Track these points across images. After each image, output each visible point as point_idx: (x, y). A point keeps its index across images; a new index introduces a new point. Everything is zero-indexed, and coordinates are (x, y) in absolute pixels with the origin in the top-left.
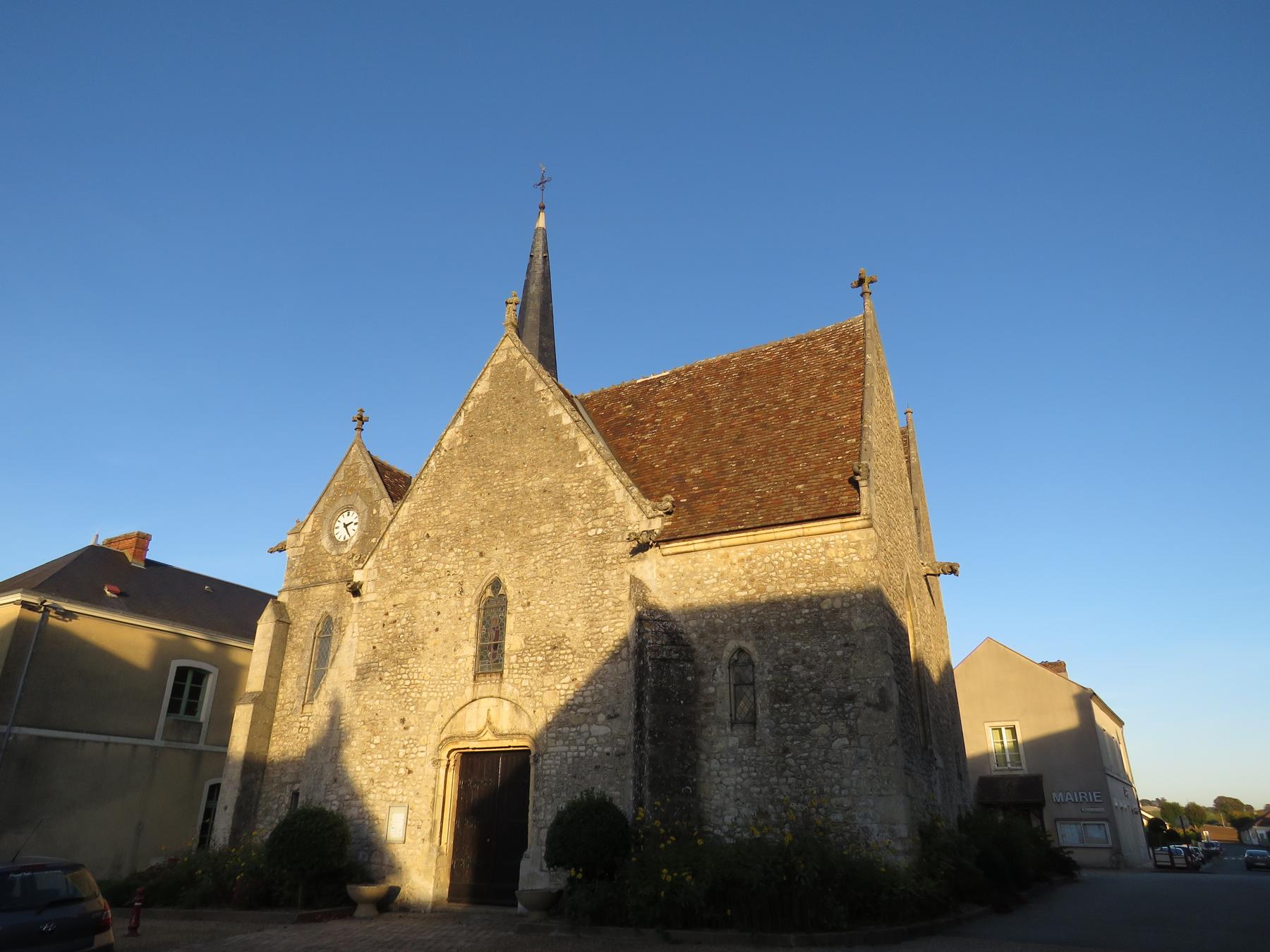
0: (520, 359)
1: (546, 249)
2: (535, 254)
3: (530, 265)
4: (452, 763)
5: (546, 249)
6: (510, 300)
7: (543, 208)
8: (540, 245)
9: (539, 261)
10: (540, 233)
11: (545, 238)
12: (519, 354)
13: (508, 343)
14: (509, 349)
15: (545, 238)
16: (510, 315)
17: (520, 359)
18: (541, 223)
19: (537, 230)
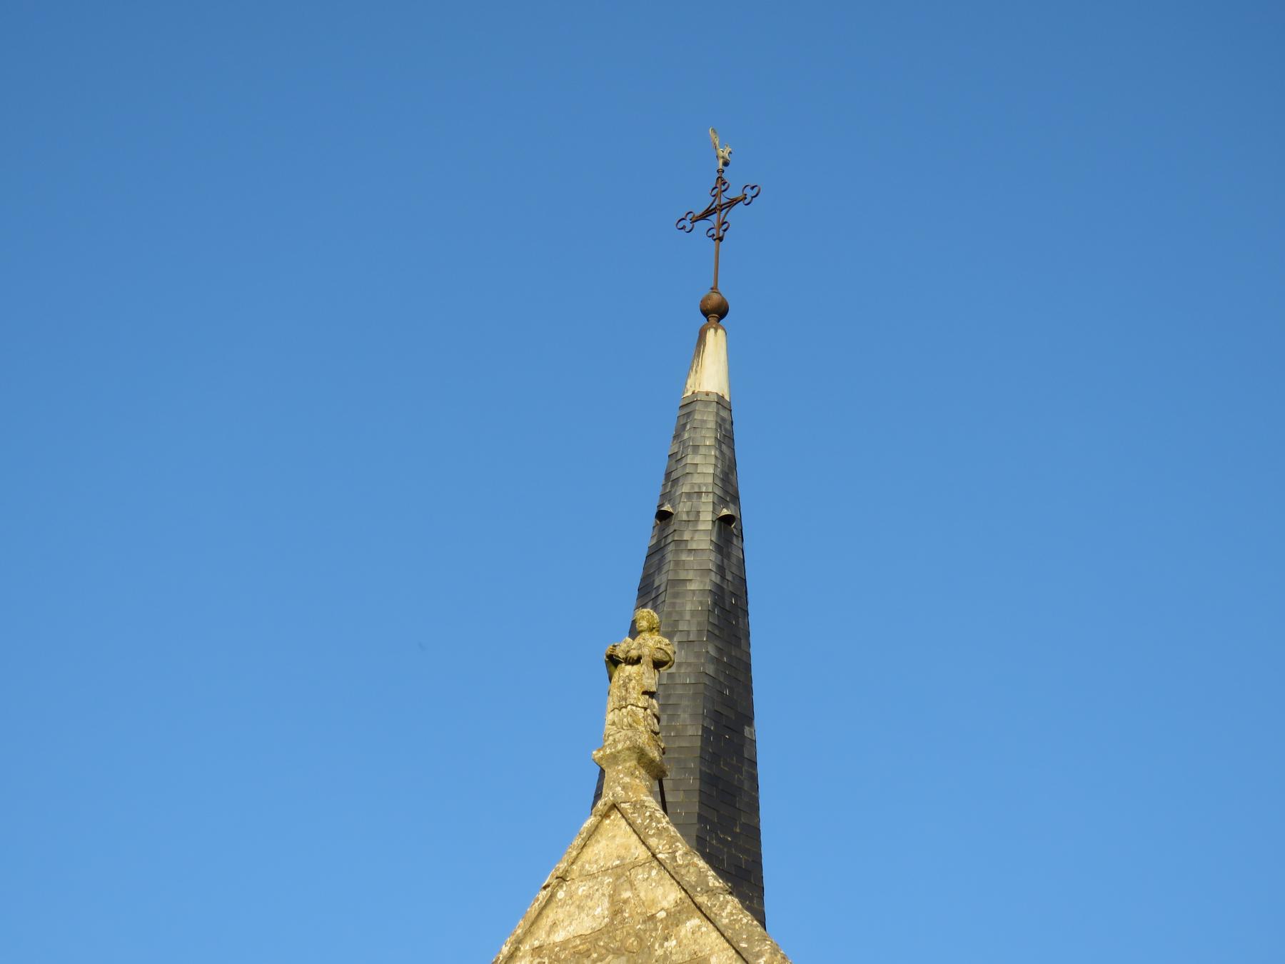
0: (675, 918)
1: (728, 490)
2: (682, 509)
3: (656, 553)
4: (578, 842)
5: (728, 490)
6: (626, 646)
7: (716, 312)
8: (703, 469)
9: (701, 536)
10: (707, 418)
11: (726, 438)
12: (669, 896)
13: (615, 841)
14: (622, 872)
15: (726, 438)
16: (625, 715)
17: (675, 918)
18: (711, 374)
19: (688, 407)
